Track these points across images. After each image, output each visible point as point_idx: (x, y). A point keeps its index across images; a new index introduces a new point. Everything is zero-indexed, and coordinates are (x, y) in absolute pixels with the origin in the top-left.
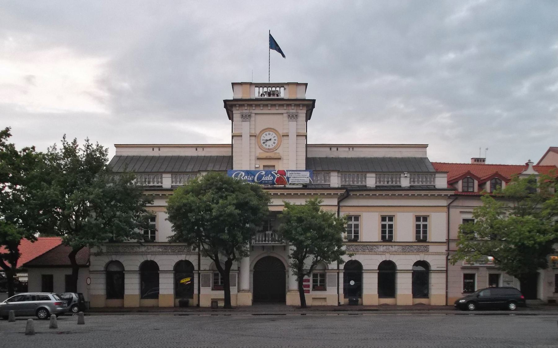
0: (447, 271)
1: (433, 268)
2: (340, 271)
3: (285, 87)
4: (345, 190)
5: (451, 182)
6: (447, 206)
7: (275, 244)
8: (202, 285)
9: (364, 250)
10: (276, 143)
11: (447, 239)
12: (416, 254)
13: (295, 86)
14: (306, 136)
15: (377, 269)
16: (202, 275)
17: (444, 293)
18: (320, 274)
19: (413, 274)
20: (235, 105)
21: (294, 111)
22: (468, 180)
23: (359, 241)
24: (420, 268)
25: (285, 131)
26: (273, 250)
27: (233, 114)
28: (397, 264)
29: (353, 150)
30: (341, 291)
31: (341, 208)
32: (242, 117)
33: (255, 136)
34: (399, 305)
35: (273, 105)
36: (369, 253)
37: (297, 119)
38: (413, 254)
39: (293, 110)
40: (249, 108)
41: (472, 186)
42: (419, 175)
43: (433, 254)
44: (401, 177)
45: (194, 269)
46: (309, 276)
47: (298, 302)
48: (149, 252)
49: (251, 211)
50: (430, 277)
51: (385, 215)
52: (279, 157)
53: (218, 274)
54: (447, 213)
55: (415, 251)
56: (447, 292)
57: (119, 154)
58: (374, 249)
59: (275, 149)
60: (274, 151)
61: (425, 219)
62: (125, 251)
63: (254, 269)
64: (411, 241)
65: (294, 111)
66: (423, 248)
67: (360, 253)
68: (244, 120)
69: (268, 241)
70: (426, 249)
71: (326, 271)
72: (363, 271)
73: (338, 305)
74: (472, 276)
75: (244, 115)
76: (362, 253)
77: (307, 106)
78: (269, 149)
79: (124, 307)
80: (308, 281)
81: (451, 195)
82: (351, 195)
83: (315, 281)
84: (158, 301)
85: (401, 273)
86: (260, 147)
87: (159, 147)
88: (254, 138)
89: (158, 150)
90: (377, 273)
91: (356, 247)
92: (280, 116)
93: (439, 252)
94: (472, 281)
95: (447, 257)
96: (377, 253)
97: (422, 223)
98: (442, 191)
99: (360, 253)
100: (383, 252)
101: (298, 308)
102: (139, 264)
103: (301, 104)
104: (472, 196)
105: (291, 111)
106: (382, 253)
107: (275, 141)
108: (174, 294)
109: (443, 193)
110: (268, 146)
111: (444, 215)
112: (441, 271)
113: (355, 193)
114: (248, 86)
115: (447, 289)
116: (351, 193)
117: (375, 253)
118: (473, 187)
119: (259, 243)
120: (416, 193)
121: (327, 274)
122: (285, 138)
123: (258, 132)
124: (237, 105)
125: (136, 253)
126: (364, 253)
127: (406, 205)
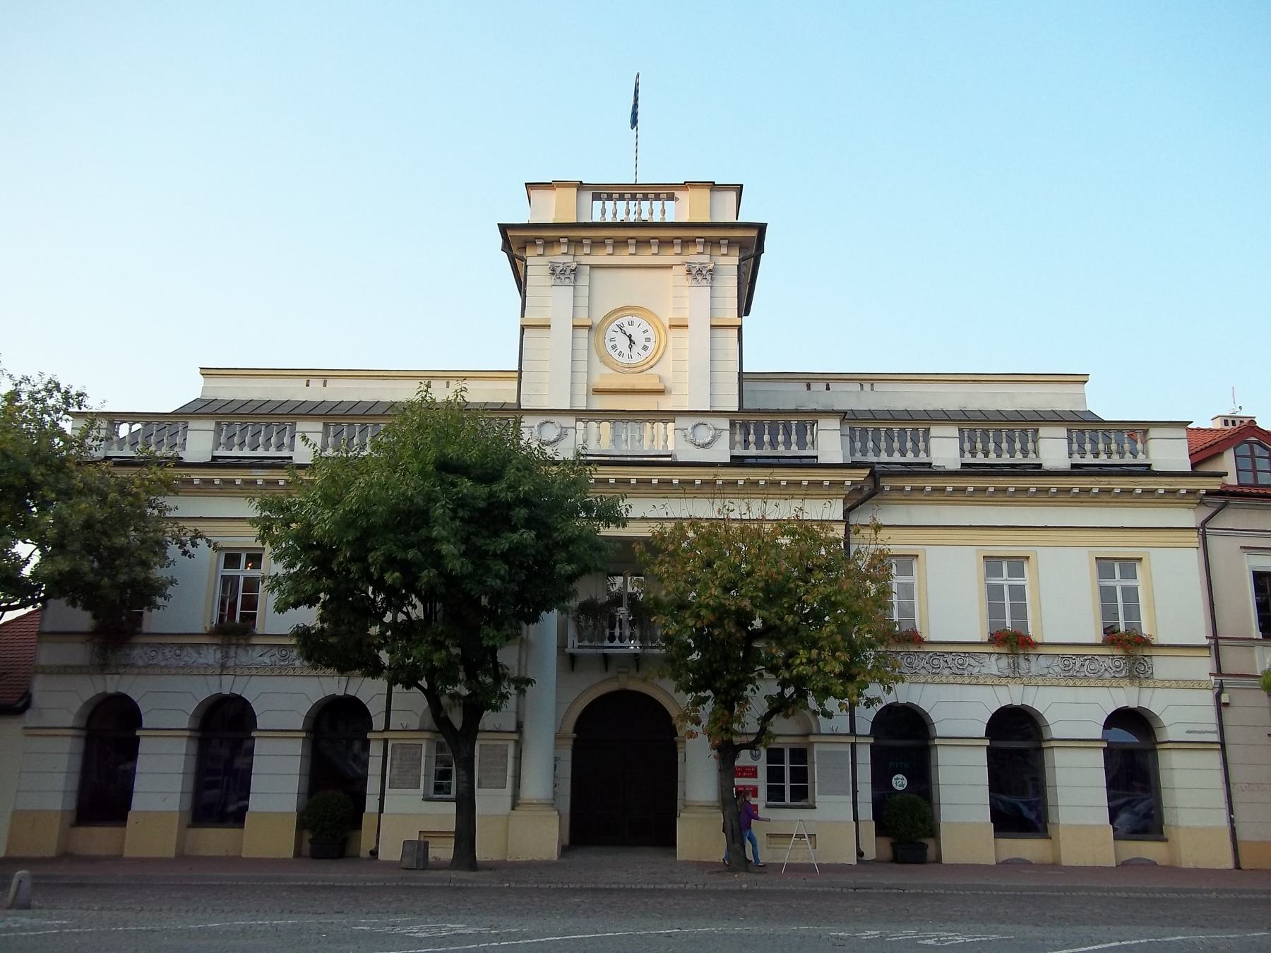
0: (1223, 745)
3: (677, 194)
4: (867, 471)
11: (1211, 635)
14: (740, 328)
15: (983, 735)
18: (792, 751)
20: (532, 242)
22: (1252, 450)
26: (638, 670)
29: (872, 390)
30: (866, 811)
32: (552, 274)
33: (590, 327)
36: (952, 681)
39: (697, 256)
43: (1167, 684)
46: (756, 757)
47: (717, 850)
50: (933, 763)
54: (1201, 549)
55: (1107, 675)
56: (1232, 821)
57: (211, 395)
61: (1129, 565)
62: (151, 662)
63: (575, 731)
68: (558, 281)
69: (621, 640)
71: (812, 739)
72: (937, 742)
76: (150, 672)
78: (630, 366)
80: (753, 773)
81: (1210, 493)
82: (887, 489)
83: (775, 775)
85: (1064, 750)
87: (325, 376)
88: (585, 332)
93: (1173, 678)
95: (1218, 697)
98: (1179, 479)
103: (724, 238)
106: (997, 682)
107: (647, 344)
108: (181, 812)
109: (1184, 485)
111: (1192, 558)
112: (1200, 746)
113: (898, 482)
115: (1231, 811)
116: (887, 484)
120: (1095, 484)
121: (816, 748)
123: (597, 319)
125: (188, 670)
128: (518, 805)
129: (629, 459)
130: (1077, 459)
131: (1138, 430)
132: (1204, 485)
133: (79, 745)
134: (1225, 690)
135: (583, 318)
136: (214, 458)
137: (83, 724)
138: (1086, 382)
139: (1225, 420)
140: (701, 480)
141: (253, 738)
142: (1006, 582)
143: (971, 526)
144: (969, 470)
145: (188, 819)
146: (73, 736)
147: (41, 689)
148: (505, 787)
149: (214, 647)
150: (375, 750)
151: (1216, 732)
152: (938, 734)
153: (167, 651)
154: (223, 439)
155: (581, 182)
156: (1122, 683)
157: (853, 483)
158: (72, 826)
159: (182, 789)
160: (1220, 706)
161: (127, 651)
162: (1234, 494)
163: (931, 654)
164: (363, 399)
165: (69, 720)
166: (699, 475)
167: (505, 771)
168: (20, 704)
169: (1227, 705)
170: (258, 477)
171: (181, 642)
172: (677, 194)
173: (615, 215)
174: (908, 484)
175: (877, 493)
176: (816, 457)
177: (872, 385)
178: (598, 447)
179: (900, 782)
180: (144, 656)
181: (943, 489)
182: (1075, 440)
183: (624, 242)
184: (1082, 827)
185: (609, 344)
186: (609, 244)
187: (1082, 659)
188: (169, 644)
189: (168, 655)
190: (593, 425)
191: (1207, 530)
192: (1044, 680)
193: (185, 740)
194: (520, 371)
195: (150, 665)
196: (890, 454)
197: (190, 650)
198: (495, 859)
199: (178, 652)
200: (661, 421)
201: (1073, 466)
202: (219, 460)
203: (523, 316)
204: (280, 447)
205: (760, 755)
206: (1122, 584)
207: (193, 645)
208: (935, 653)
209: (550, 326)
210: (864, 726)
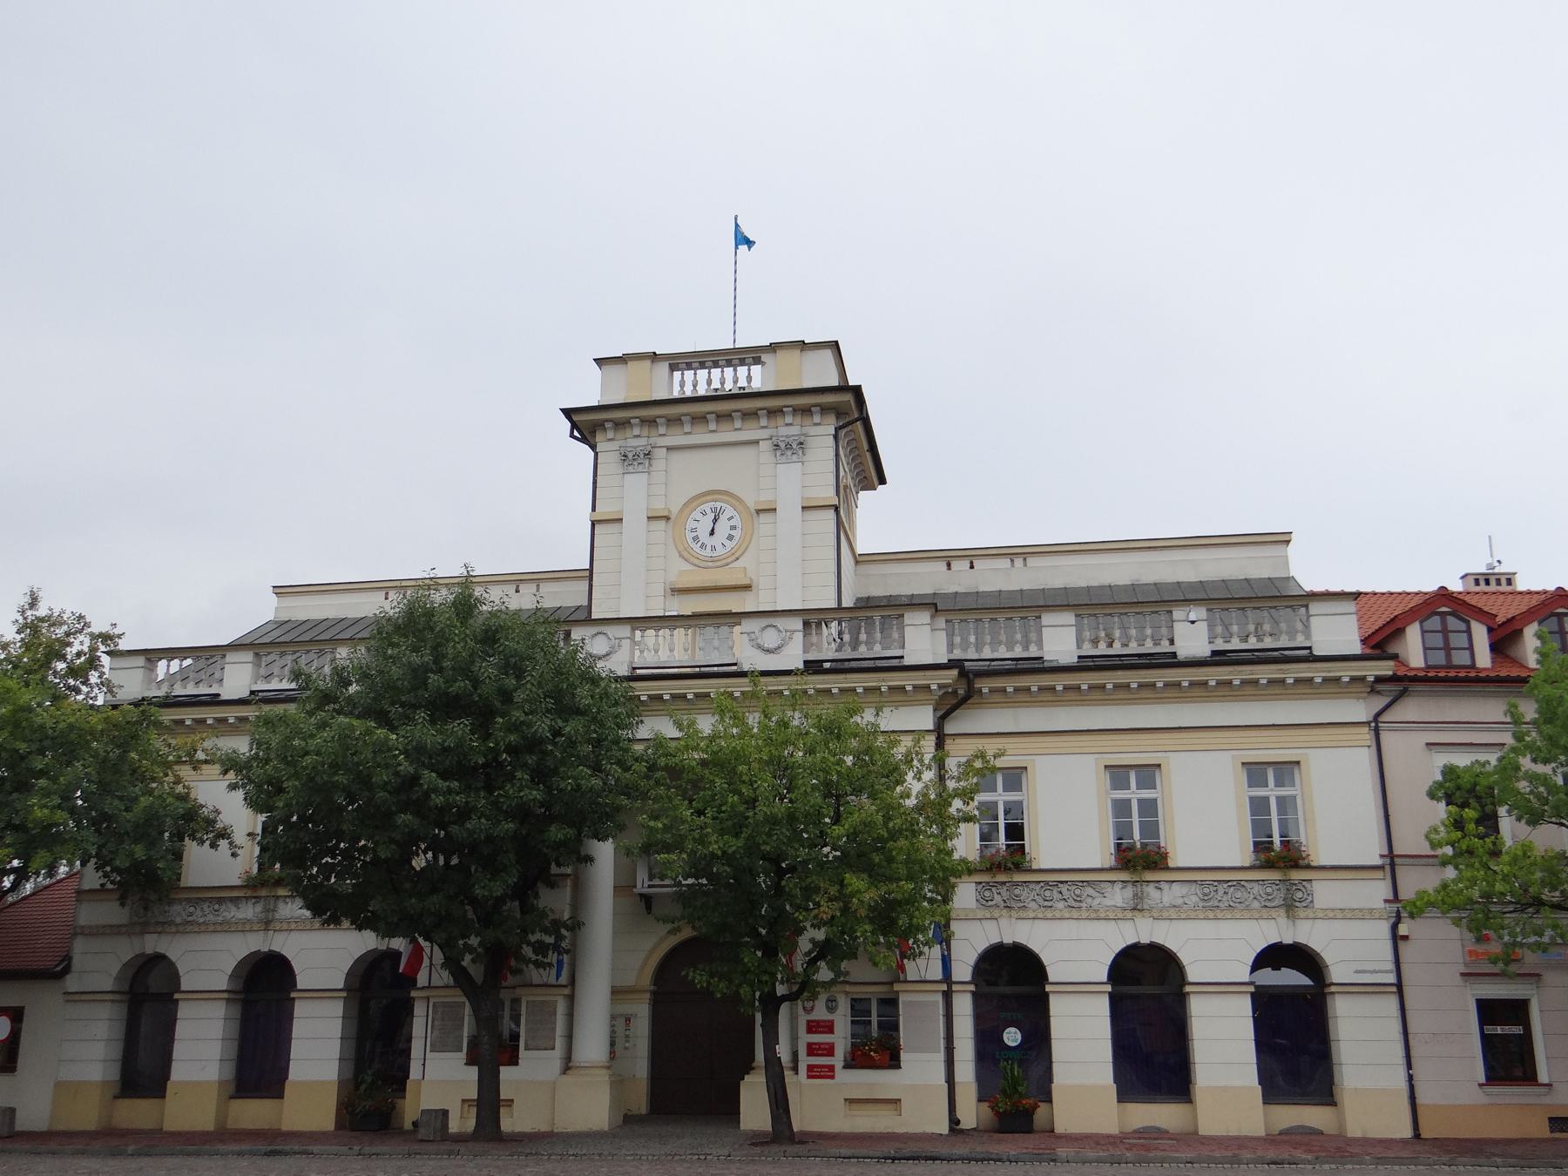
0: (1399, 986)
1: (1338, 972)
3: (764, 357)
4: (955, 672)
5: (1378, 638)
9: (1046, 903)
10: (737, 538)
11: (1386, 852)
13: (797, 352)
15: (1105, 979)
17: (1403, 1084)
19: (1256, 998)
22: (1444, 623)
24: (1290, 977)
25: (765, 498)
29: (1025, 565)
31: (948, 741)
33: (668, 518)
35: (723, 417)
36: (1067, 915)
37: (804, 454)
39: (789, 428)
41: (1466, 646)
43: (1331, 915)
45: (1048, 980)
49: (552, 767)
50: (1330, 1014)
52: (746, 582)
53: (464, 1003)
55: (1256, 904)
56: (1411, 1078)
57: (284, 617)
58: (1090, 900)
59: (733, 558)
61: (1286, 770)
62: (190, 919)
67: (1032, 915)
71: (897, 987)
73: (951, 1129)
74: (1516, 1011)
75: (630, 455)
76: (988, 916)
77: (838, 411)
79: (1196, 1133)
80: (829, 1028)
81: (1379, 680)
82: (985, 690)
84: (1195, 1111)
86: (685, 554)
88: (661, 524)
89: (945, 567)
90: (1107, 995)
92: (749, 452)
93: (1355, 907)
94: (1517, 1030)
95: (1394, 928)
96: (1102, 916)
97: (1272, 792)
101: (762, 1144)
102: (115, 968)
103: (816, 406)
104: (1467, 680)
105: (784, 431)
106: (1120, 916)
107: (733, 532)
109: (1346, 672)
110: (709, 548)
111: (1363, 758)
112: (1372, 989)
113: (998, 683)
114: (647, 363)
115: (1409, 1066)
116: (985, 685)
118: (1471, 648)
120: (1237, 674)
121: (902, 998)
122: (764, 517)
125: (226, 927)
126: (1049, 916)
127: (1149, 727)
129: (716, 669)
130: (1220, 645)
132: (1385, 668)
133: (236, 1011)
134: (1403, 920)
135: (659, 506)
137: (126, 987)
138: (1288, 542)
139: (1507, 579)
141: (294, 999)
142: (1134, 796)
143: (1274, 725)
145: (232, 1089)
147: (80, 949)
148: (553, 1049)
149: (253, 900)
151: (1390, 972)
153: (205, 907)
155: (654, 353)
156: (1274, 913)
157: (940, 686)
158: (115, 1097)
159: (221, 1057)
160: (1397, 939)
161: (167, 908)
162: (1415, 679)
163: (1042, 884)
165: (223, 984)
166: (691, 689)
167: (554, 1030)
168: (59, 969)
169: (1405, 938)
170: (665, 692)
171: (218, 896)
172: (764, 357)
173: (695, 386)
174: (1010, 684)
175: (972, 697)
177: (1025, 559)
178: (656, 659)
179: (1012, 1037)
181: (1053, 689)
183: (754, 414)
184: (1225, 1089)
185: (690, 536)
186: (636, 425)
190: (651, 632)
191: (1380, 725)
192: (1178, 913)
193: (224, 1002)
194: (591, 570)
197: (230, 905)
198: (543, 1130)
200: (725, 624)
201: (1214, 653)
202: (260, 694)
203: (594, 509)
206: (1139, 796)
207: (232, 900)
208: (1047, 883)
209: (775, 509)
210: (963, 970)
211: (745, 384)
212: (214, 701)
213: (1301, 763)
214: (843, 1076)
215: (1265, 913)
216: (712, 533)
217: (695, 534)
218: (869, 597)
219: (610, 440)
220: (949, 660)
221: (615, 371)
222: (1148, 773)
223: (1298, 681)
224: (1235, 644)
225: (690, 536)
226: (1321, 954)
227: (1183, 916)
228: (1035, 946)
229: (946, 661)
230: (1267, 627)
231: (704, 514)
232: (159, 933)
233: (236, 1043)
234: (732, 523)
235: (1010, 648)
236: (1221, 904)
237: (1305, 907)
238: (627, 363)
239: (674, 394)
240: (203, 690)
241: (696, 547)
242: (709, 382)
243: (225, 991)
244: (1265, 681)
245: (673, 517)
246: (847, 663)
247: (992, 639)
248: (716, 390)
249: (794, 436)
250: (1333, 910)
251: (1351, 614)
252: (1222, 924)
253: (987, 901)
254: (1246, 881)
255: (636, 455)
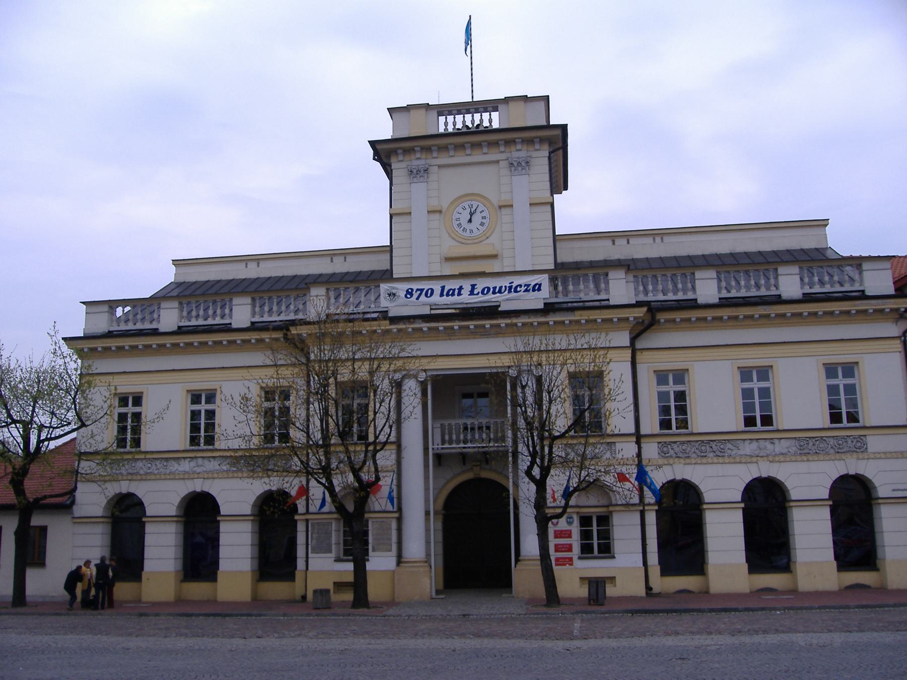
2: (646, 508)
4: (645, 309)
6: (899, 337)
7: (464, 448)
8: (312, 549)
9: (702, 454)
12: (836, 459)
16: (312, 524)
20: (394, 152)
21: (523, 154)
23: (862, 425)
25: (505, 198)
27: (392, 170)
28: (789, 484)
33: (440, 212)
34: (807, 590)
36: (716, 461)
38: (827, 458)
39: (519, 153)
40: (424, 156)
42: (810, 270)
43: (878, 456)
44: (863, 271)
45: (220, 513)
47: (540, 590)
48: (199, 473)
51: (765, 366)
52: (494, 253)
60: (481, 242)
62: (149, 471)
64: (733, 428)
65: (421, 163)
66: (852, 442)
70: (859, 444)
71: (611, 509)
73: (647, 593)
75: (415, 171)
76: (666, 462)
77: (550, 141)
80: (568, 534)
82: (662, 321)
83: (586, 535)
88: (437, 216)
89: (611, 243)
91: (684, 447)
92: (492, 169)
93: (893, 451)
97: (756, 385)
99: (710, 461)
100: (751, 456)
103: (536, 137)
105: (516, 154)
106: (749, 460)
107: (484, 221)
108: (253, 571)
114: (423, 111)
116: (662, 317)
117: (732, 461)
119: (466, 446)
122: (504, 211)
124: (399, 151)
128: (519, 560)
131: (858, 262)
133: (181, 528)
135: (434, 204)
136: (253, 323)
138: (826, 225)
140: (443, 326)
143: (174, 370)
144: (725, 303)
145: (181, 575)
146: (176, 521)
149: (189, 460)
150: (301, 527)
152: (793, 498)
154: (185, 314)
157: (635, 318)
164: (337, 271)
167: (390, 539)
168: (68, 502)
171: (168, 456)
174: (678, 316)
176: (608, 300)
180: (143, 467)
182: (723, 279)
186: (418, 151)
187: (814, 440)
188: (159, 459)
189: (159, 466)
192: (783, 457)
193: (250, 522)
195: (149, 473)
196: (685, 293)
197: (173, 462)
199: (165, 464)
204: (223, 317)
205: (573, 522)
207: (174, 459)
208: (703, 441)
209: (512, 206)
211: (488, 125)
212: (155, 332)
213: (774, 367)
214: (578, 564)
215: (838, 456)
216: (470, 221)
217: (459, 222)
218: (361, 271)
219: (468, 155)
220: (636, 302)
221: (400, 117)
222: (764, 373)
223: (875, 311)
224: (817, 289)
225: (456, 223)
226: (873, 480)
227: (788, 460)
228: (695, 480)
229: (635, 303)
230: (836, 278)
231: (464, 209)
232: (130, 480)
233: (790, 533)
234: (483, 214)
235: (685, 293)
236: (811, 452)
237: (862, 452)
238: (409, 111)
239: (449, 131)
240: (147, 326)
241: (460, 231)
242: (454, 124)
243: (102, 517)
244: (838, 312)
245: (444, 210)
246: (570, 304)
247: (653, 288)
248: (458, 129)
249: (522, 157)
250: (879, 453)
251: (104, 312)
252: (813, 464)
253: (665, 454)
254: (826, 437)
255: (418, 171)
